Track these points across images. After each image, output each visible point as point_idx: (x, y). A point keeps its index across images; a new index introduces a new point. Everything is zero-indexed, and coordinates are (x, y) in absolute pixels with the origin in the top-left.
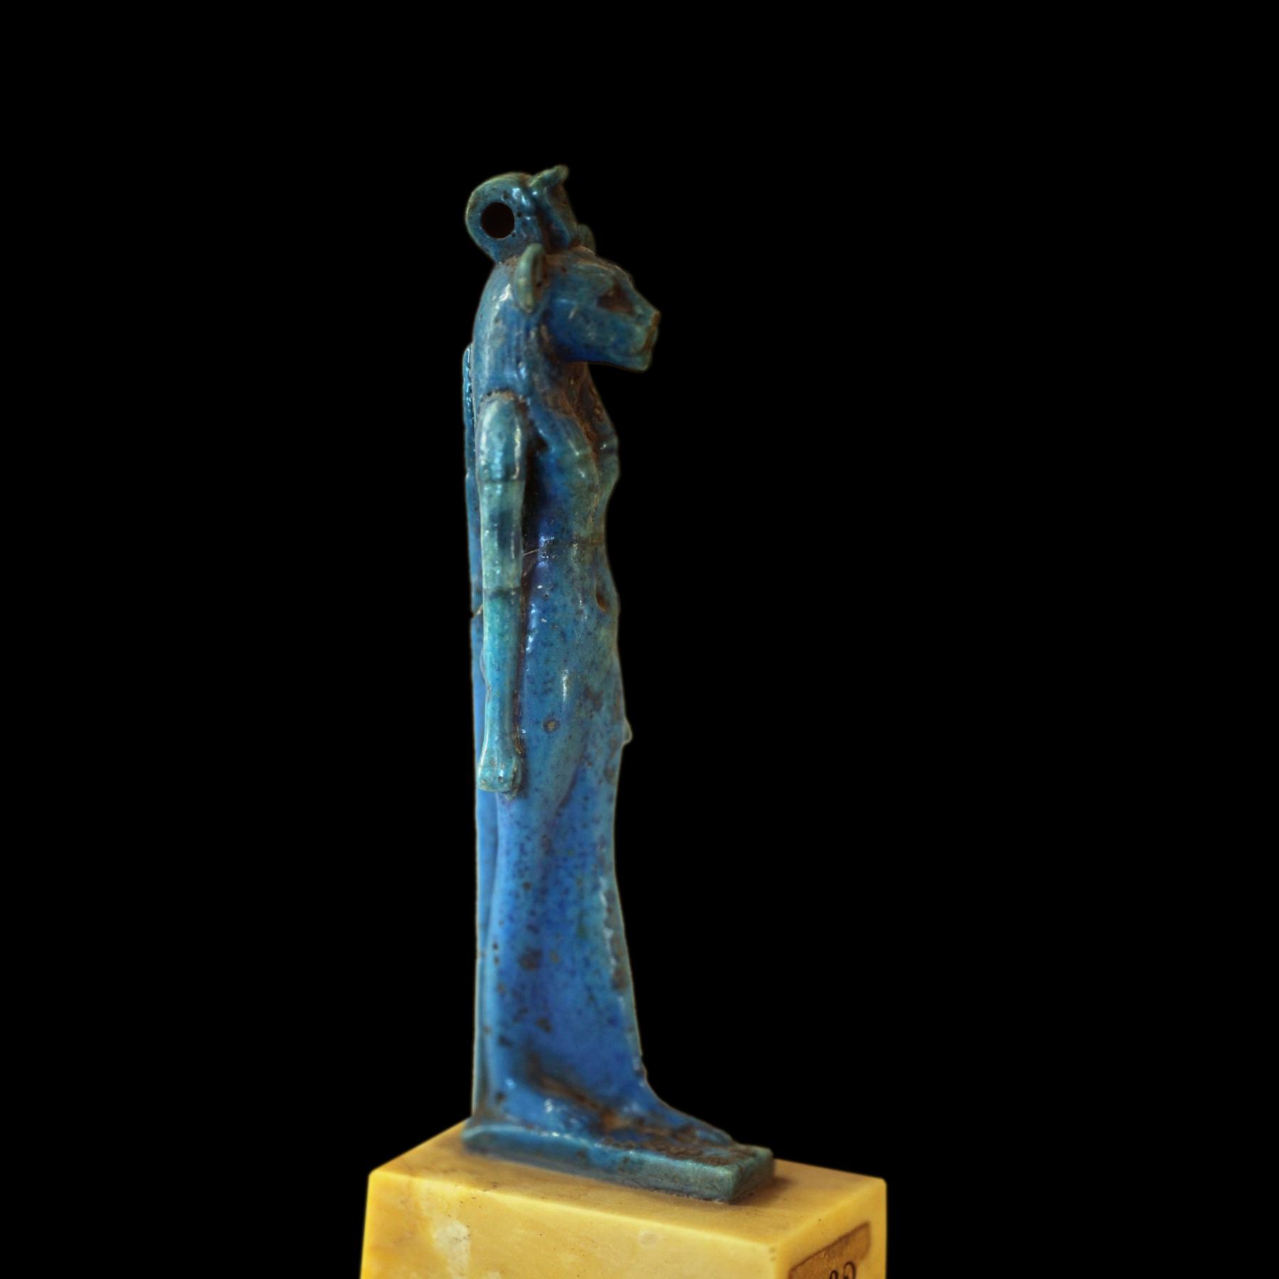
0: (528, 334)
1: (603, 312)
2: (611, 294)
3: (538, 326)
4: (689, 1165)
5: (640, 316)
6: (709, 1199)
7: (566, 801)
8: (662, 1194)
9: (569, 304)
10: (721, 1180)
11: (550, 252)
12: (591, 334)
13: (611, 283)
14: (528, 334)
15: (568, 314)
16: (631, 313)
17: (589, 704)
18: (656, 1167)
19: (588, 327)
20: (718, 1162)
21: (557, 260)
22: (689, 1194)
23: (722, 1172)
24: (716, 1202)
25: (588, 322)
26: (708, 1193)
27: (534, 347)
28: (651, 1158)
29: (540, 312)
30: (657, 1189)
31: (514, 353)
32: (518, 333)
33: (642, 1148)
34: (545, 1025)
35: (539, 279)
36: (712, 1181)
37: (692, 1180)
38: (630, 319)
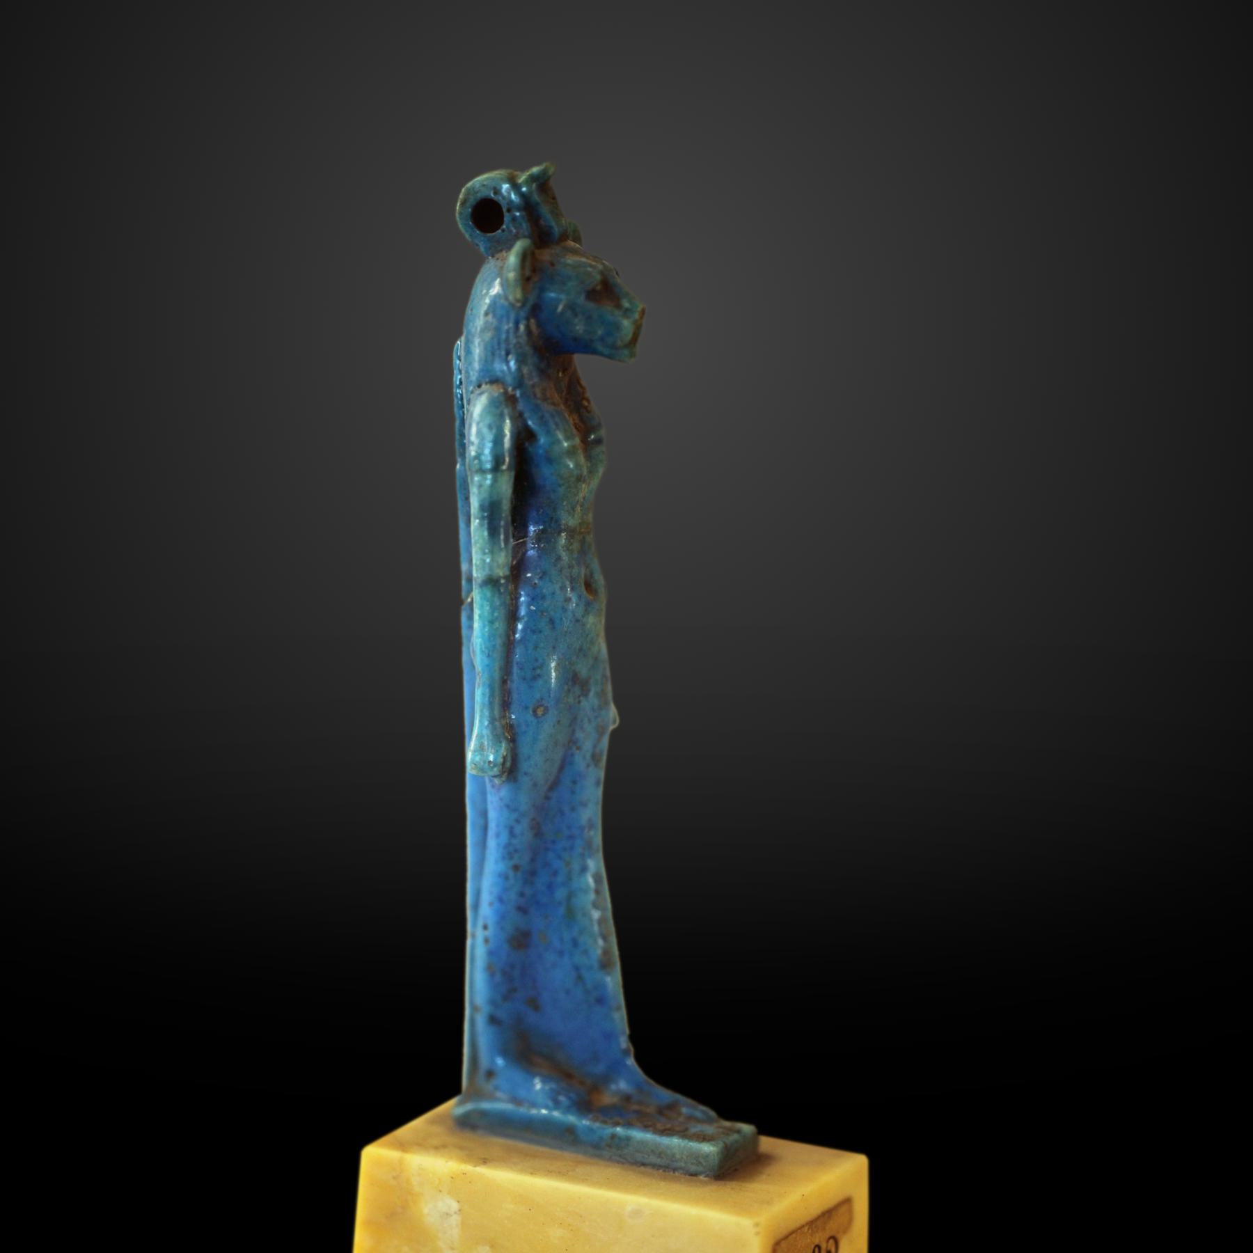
0: (517, 328)
1: (591, 305)
2: (599, 288)
3: (528, 319)
4: (675, 1142)
5: (627, 310)
6: (694, 1175)
7: (554, 785)
8: (649, 1170)
9: (558, 298)
10: (707, 1156)
11: (538, 247)
14: (517, 328)
15: (556, 308)
16: (619, 306)
17: (577, 690)
18: (643, 1143)
19: (576, 321)
20: (704, 1138)
21: (546, 255)
22: (675, 1170)
23: (707, 1148)
24: (702, 1177)
25: (576, 315)
26: (693, 1168)
27: (523, 340)
28: (638, 1135)
29: (529, 305)
30: (644, 1164)
31: (503, 346)
32: (508, 326)
33: (629, 1125)
34: (534, 1004)
35: (528, 273)
36: (697, 1157)
37: (678, 1156)
38: (617, 312)
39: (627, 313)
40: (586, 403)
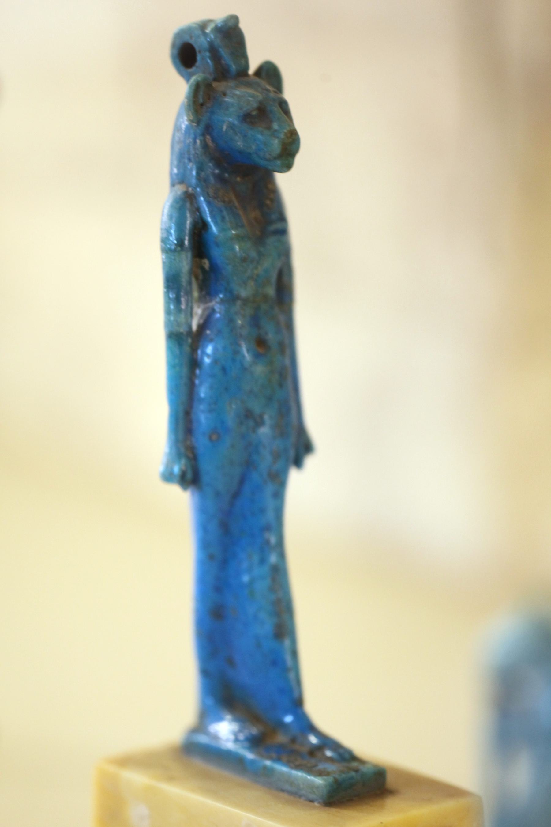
0: (195, 142)
1: (245, 127)
2: (254, 113)
3: (203, 135)
4: (299, 774)
5: (276, 131)
6: (312, 801)
7: (236, 495)
8: (285, 795)
9: (227, 119)
10: (318, 787)
11: (215, 80)
12: (240, 144)
13: (255, 105)
14: (195, 142)
15: (222, 128)
16: (269, 128)
17: (251, 423)
18: (282, 774)
19: (237, 138)
20: (320, 774)
21: (220, 86)
22: (300, 796)
23: (318, 781)
24: (316, 804)
25: (236, 134)
26: (311, 796)
27: (199, 151)
28: (282, 769)
29: (202, 125)
30: (283, 790)
31: (186, 156)
32: (190, 140)
33: (278, 760)
34: (231, 662)
35: (201, 101)
36: (312, 787)
37: (301, 786)
38: (267, 132)
39: (274, 134)
40: (268, 202)
